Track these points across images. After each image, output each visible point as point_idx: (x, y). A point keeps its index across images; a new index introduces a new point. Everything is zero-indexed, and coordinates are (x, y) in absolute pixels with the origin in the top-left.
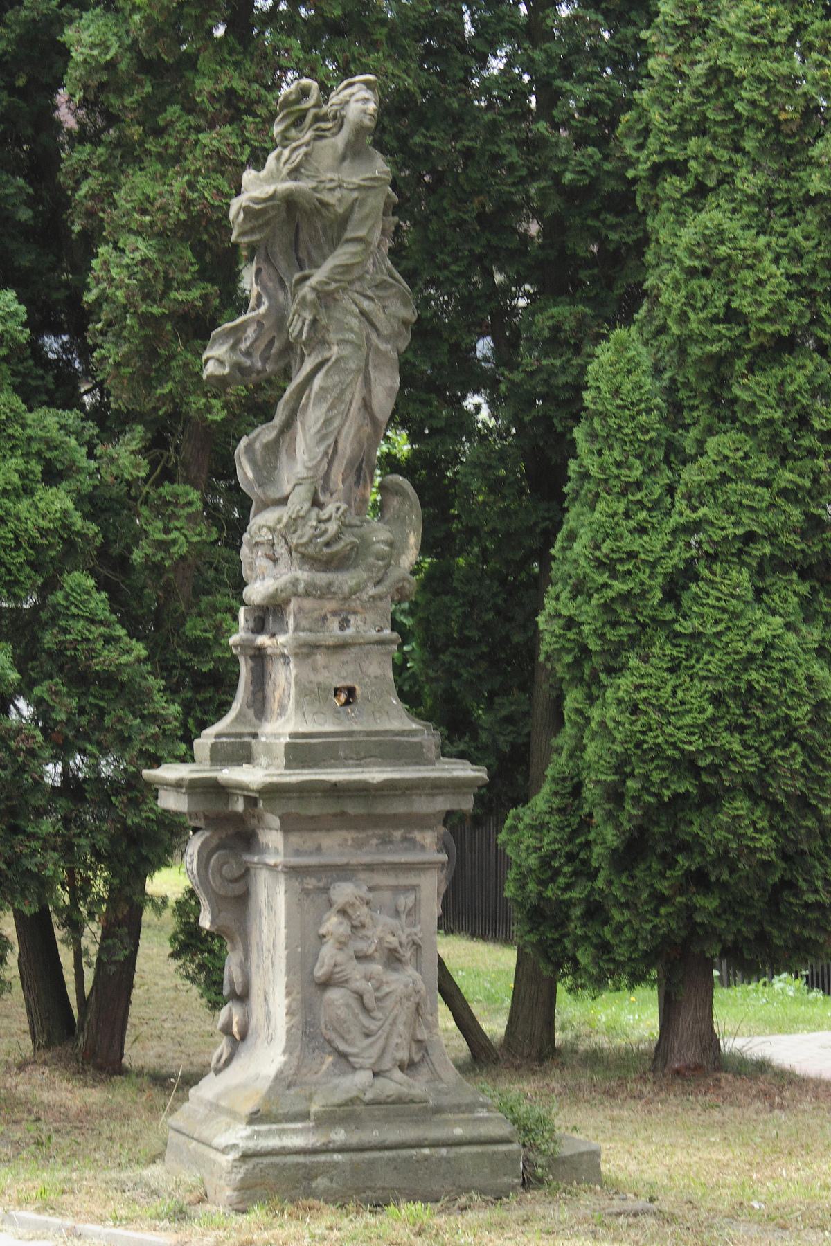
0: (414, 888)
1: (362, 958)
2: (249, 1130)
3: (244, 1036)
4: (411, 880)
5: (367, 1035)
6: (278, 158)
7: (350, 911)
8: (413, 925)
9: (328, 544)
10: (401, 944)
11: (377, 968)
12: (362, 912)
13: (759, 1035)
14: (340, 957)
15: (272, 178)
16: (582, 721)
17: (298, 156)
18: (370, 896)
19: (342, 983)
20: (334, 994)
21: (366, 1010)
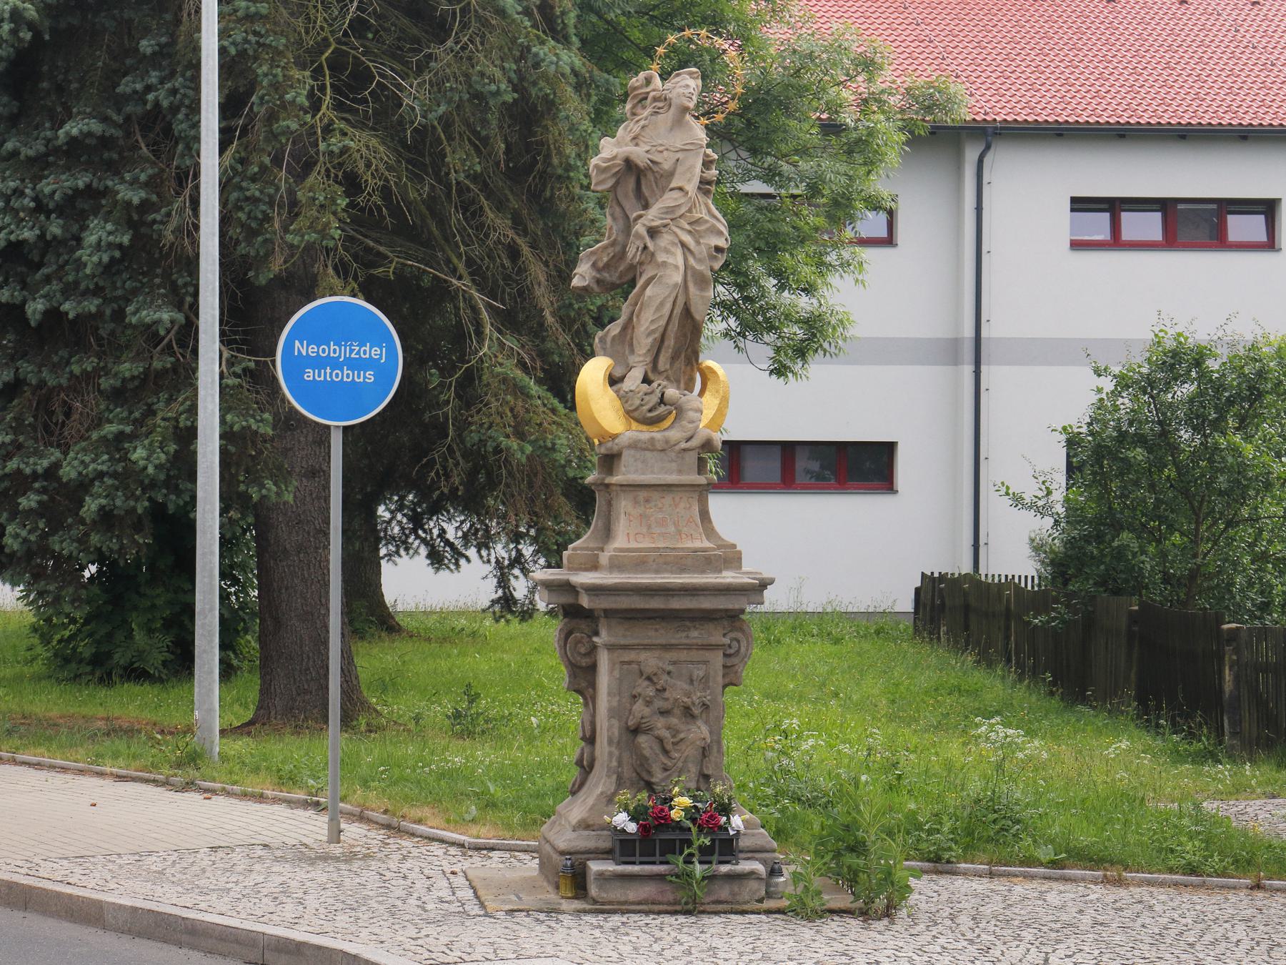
0: (706, 662)
1: (664, 713)
2: (574, 835)
3: (591, 766)
4: (708, 655)
5: (666, 770)
6: (625, 128)
7: (655, 679)
8: (704, 690)
9: (650, 411)
10: (693, 704)
11: (674, 721)
12: (663, 680)
13: (594, 805)
14: (647, 711)
15: (618, 144)
16: (755, 267)
17: (637, 129)
18: (670, 668)
19: (648, 731)
20: (642, 739)
21: (666, 752)
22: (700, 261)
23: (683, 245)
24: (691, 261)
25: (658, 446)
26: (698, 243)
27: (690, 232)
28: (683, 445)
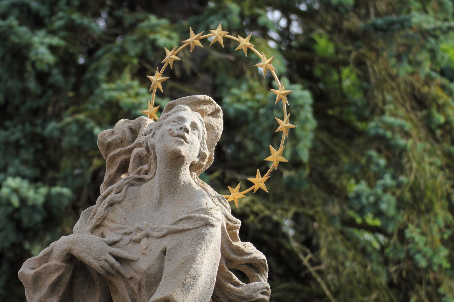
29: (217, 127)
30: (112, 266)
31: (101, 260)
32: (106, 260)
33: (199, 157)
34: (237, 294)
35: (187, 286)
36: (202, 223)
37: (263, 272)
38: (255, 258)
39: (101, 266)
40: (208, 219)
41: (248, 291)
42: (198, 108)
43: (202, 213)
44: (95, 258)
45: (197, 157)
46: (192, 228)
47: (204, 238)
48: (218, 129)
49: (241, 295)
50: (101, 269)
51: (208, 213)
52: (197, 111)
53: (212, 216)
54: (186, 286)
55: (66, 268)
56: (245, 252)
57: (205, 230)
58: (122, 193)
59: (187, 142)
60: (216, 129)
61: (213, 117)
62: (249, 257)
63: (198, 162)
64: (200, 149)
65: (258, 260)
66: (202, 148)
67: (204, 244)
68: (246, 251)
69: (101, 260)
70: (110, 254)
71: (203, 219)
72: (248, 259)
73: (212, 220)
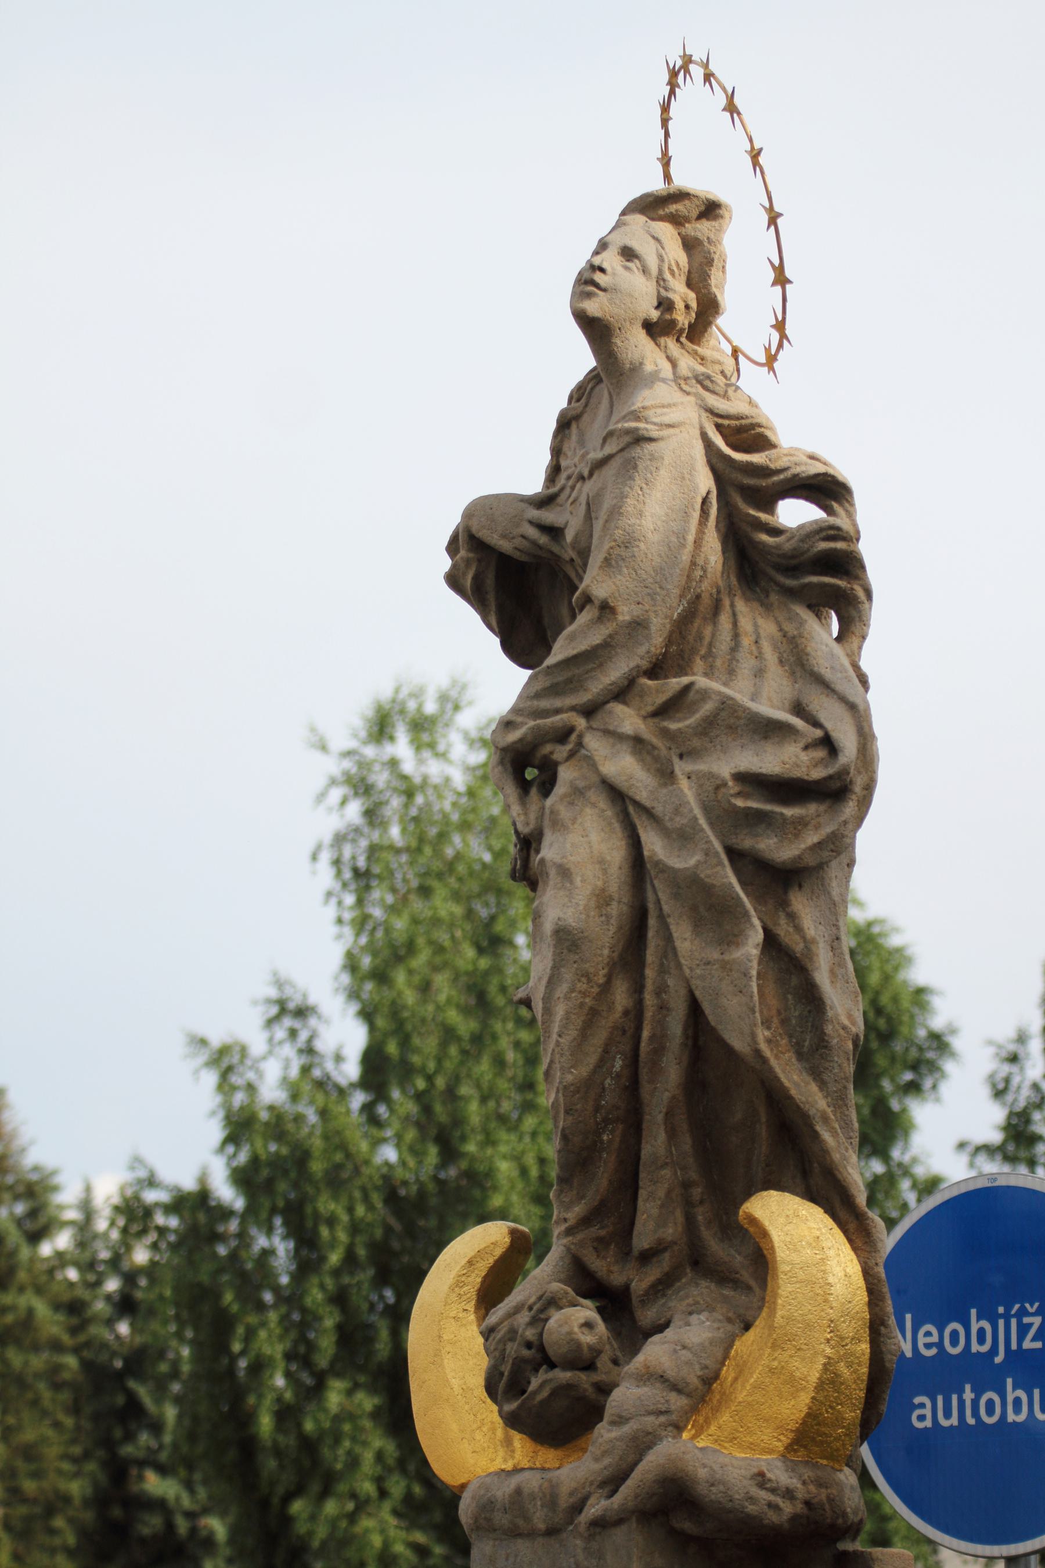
22: (683, 837)
23: (617, 796)
24: (653, 844)
25: (539, 1519)
26: (667, 776)
27: (637, 742)
28: (596, 1507)
29: (708, 238)
30: (534, 543)
31: (513, 538)
32: (523, 536)
33: (661, 309)
34: (774, 551)
35: (617, 562)
36: (627, 439)
37: (843, 496)
38: (795, 476)
39: (516, 548)
40: (637, 429)
41: (793, 541)
42: (661, 212)
43: (630, 420)
44: (504, 536)
45: (657, 308)
46: (614, 451)
47: (635, 467)
48: (709, 242)
49: (780, 552)
50: (518, 553)
51: (638, 419)
52: (661, 219)
53: (647, 422)
54: (613, 562)
55: (479, 561)
56: (771, 470)
57: (636, 452)
58: (583, 401)
59: (604, 290)
60: (706, 244)
61: (708, 219)
62: (782, 477)
63: (659, 318)
64: (659, 292)
65: (803, 478)
66: (662, 291)
67: (637, 478)
68: (772, 466)
69: (513, 538)
70: (531, 522)
71: (628, 432)
72: (781, 481)
73: (647, 429)
